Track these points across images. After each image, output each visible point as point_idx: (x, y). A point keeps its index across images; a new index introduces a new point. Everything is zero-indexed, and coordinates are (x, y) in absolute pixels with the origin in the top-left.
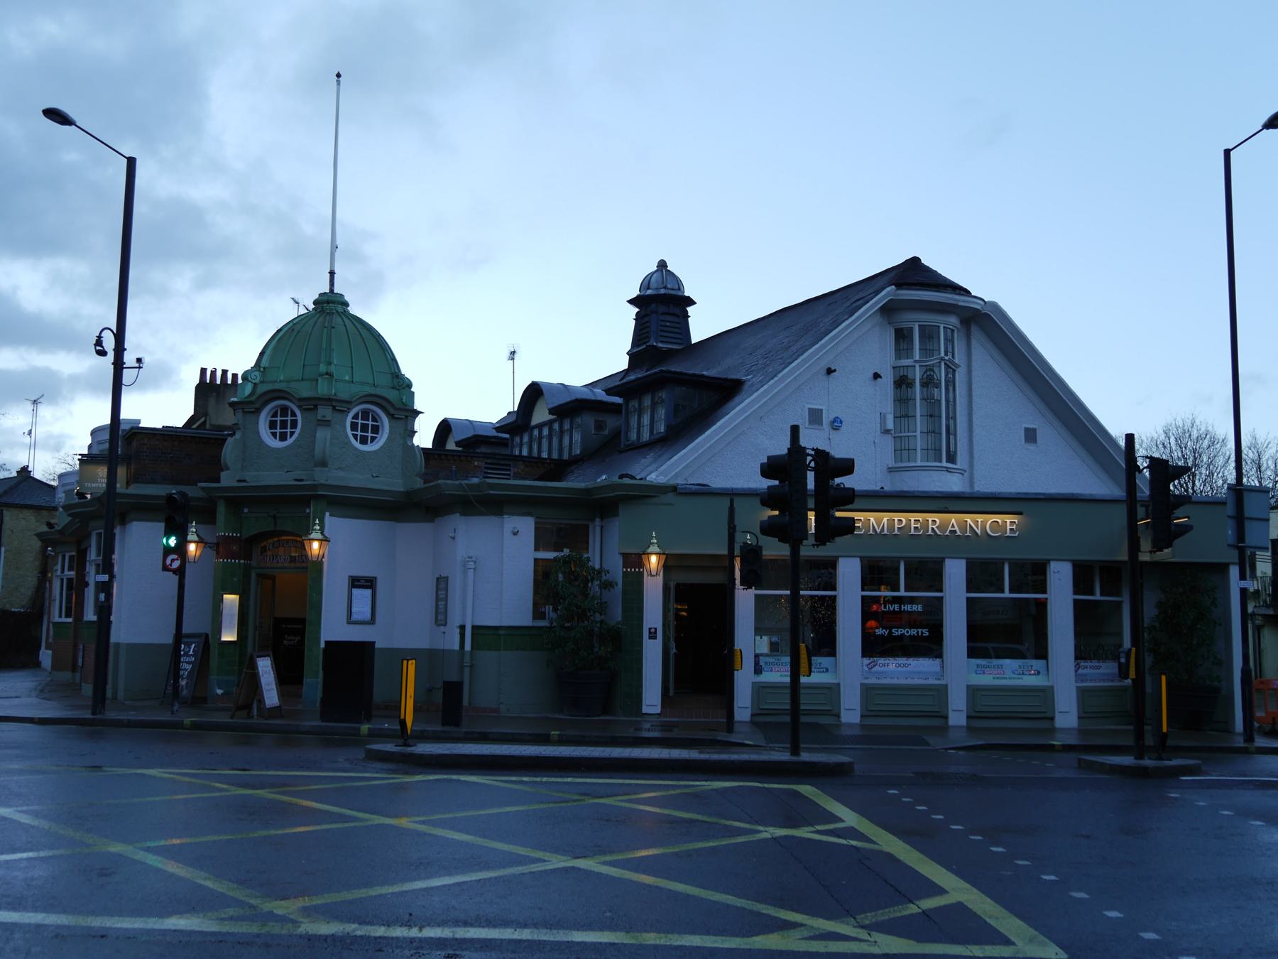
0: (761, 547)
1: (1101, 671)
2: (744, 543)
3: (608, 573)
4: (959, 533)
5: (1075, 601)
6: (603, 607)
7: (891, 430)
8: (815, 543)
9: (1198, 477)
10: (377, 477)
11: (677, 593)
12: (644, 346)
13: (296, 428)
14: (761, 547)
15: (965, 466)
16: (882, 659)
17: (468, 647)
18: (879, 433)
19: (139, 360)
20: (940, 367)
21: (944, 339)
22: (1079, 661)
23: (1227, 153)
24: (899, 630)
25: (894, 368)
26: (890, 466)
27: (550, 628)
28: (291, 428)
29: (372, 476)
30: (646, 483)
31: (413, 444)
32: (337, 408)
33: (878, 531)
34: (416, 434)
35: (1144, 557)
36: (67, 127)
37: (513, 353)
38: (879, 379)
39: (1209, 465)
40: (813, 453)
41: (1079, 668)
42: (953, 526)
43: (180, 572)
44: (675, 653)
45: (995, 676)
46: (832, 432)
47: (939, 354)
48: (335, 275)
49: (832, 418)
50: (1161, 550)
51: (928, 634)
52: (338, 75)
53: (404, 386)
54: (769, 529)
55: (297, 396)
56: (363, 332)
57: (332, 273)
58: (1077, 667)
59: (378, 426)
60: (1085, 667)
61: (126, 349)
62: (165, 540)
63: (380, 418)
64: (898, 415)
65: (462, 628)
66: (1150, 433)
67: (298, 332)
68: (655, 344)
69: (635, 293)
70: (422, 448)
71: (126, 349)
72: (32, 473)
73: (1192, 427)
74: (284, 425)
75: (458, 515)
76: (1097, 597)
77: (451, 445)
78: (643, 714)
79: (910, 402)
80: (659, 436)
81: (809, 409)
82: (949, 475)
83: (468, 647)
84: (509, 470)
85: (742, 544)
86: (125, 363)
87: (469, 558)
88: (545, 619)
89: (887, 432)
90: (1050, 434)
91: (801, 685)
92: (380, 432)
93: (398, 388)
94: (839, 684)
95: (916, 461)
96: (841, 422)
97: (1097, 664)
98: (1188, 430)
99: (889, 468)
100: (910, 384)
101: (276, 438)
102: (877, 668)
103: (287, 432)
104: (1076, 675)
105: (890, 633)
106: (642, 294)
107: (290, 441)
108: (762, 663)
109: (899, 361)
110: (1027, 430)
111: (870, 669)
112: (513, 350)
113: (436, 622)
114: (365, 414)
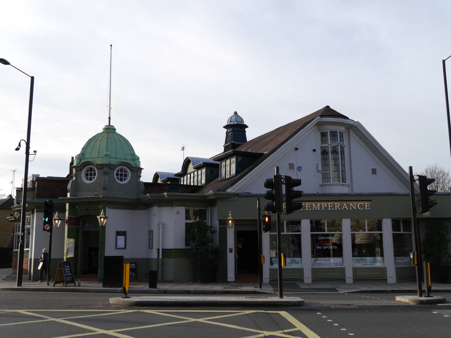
0: (270, 216)
1: (405, 260)
2: (264, 215)
3: (213, 227)
4: (347, 209)
5: (393, 234)
6: (212, 241)
7: (321, 171)
8: (286, 213)
9: (439, 187)
10: (126, 193)
11: (239, 235)
12: (229, 143)
13: (95, 176)
14: (270, 216)
15: (350, 184)
16: (320, 258)
17: (160, 257)
18: (316, 172)
19: (35, 152)
20: (338, 146)
21: (340, 136)
22: (396, 257)
23: (444, 61)
24: (326, 247)
25: (321, 147)
26: (321, 184)
27: (192, 249)
28: (94, 176)
29: (125, 193)
30: (226, 193)
31: (140, 181)
32: (111, 168)
33: (316, 209)
34: (141, 177)
35: (418, 216)
36: (7, 65)
37: (183, 148)
38: (315, 151)
39: (443, 183)
40: (284, 177)
41: (396, 260)
42: (345, 206)
43: (50, 230)
44: (237, 258)
45: (363, 264)
46: (298, 172)
47: (338, 141)
48: (111, 119)
49: (298, 166)
50: (425, 212)
51: (337, 248)
52: (111, 46)
53: (136, 159)
54: (269, 208)
55: (96, 164)
56: (121, 140)
57: (110, 118)
58: (395, 259)
59: (126, 174)
60: (398, 259)
61: (30, 148)
62: (44, 219)
63: (127, 171)
64: (323, 165)
65: (158, 250)
66: (420, 172)
67: (97, 140)
68: (233, 142)
69: (226, 124)
70: (143, 182)
71: (30, 148)
72: (13, 197)
73: (436, 169)
74: (121, 175)
75: (156, 207)
76: (402, 232)
77: (159, 181)
78: (228, 281)
79: (328, 160)
80: (233, 175)
81: (289, 163)
82: (343, 187)
83: (160, 257)
84: (178, 190)
85: (263, 215)
86: (30, 153)
87: (160, 223)
88: (190, 246)
89: (319, 171)
90: (381, 170)
91: (282, 269)
92: (127, 176)
93: (134, 160)
94: (303, 268)
95: (330, 182)
96: (301, 168)
97: (403, 258)
98: (434, 170)
99: (320, 185)
100: (327, 153)
101: (88, 179)
102: (318, 262)
103: (90, 176)
104: (395, 263)
105: (322, 248)
106: (228, 124)
107: (93, 181)
108: (273, 261)
109: (322, 145)
110: (372, 169)
111: (315, 262)
112: (183, 147)
113: (149, 248)
114: (122, 170)
